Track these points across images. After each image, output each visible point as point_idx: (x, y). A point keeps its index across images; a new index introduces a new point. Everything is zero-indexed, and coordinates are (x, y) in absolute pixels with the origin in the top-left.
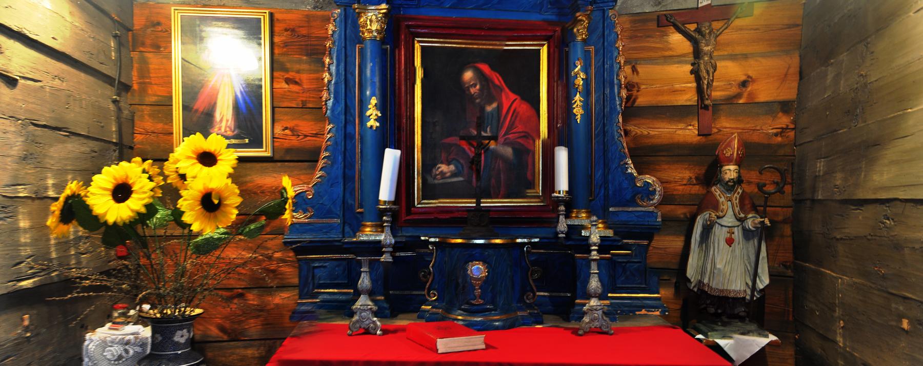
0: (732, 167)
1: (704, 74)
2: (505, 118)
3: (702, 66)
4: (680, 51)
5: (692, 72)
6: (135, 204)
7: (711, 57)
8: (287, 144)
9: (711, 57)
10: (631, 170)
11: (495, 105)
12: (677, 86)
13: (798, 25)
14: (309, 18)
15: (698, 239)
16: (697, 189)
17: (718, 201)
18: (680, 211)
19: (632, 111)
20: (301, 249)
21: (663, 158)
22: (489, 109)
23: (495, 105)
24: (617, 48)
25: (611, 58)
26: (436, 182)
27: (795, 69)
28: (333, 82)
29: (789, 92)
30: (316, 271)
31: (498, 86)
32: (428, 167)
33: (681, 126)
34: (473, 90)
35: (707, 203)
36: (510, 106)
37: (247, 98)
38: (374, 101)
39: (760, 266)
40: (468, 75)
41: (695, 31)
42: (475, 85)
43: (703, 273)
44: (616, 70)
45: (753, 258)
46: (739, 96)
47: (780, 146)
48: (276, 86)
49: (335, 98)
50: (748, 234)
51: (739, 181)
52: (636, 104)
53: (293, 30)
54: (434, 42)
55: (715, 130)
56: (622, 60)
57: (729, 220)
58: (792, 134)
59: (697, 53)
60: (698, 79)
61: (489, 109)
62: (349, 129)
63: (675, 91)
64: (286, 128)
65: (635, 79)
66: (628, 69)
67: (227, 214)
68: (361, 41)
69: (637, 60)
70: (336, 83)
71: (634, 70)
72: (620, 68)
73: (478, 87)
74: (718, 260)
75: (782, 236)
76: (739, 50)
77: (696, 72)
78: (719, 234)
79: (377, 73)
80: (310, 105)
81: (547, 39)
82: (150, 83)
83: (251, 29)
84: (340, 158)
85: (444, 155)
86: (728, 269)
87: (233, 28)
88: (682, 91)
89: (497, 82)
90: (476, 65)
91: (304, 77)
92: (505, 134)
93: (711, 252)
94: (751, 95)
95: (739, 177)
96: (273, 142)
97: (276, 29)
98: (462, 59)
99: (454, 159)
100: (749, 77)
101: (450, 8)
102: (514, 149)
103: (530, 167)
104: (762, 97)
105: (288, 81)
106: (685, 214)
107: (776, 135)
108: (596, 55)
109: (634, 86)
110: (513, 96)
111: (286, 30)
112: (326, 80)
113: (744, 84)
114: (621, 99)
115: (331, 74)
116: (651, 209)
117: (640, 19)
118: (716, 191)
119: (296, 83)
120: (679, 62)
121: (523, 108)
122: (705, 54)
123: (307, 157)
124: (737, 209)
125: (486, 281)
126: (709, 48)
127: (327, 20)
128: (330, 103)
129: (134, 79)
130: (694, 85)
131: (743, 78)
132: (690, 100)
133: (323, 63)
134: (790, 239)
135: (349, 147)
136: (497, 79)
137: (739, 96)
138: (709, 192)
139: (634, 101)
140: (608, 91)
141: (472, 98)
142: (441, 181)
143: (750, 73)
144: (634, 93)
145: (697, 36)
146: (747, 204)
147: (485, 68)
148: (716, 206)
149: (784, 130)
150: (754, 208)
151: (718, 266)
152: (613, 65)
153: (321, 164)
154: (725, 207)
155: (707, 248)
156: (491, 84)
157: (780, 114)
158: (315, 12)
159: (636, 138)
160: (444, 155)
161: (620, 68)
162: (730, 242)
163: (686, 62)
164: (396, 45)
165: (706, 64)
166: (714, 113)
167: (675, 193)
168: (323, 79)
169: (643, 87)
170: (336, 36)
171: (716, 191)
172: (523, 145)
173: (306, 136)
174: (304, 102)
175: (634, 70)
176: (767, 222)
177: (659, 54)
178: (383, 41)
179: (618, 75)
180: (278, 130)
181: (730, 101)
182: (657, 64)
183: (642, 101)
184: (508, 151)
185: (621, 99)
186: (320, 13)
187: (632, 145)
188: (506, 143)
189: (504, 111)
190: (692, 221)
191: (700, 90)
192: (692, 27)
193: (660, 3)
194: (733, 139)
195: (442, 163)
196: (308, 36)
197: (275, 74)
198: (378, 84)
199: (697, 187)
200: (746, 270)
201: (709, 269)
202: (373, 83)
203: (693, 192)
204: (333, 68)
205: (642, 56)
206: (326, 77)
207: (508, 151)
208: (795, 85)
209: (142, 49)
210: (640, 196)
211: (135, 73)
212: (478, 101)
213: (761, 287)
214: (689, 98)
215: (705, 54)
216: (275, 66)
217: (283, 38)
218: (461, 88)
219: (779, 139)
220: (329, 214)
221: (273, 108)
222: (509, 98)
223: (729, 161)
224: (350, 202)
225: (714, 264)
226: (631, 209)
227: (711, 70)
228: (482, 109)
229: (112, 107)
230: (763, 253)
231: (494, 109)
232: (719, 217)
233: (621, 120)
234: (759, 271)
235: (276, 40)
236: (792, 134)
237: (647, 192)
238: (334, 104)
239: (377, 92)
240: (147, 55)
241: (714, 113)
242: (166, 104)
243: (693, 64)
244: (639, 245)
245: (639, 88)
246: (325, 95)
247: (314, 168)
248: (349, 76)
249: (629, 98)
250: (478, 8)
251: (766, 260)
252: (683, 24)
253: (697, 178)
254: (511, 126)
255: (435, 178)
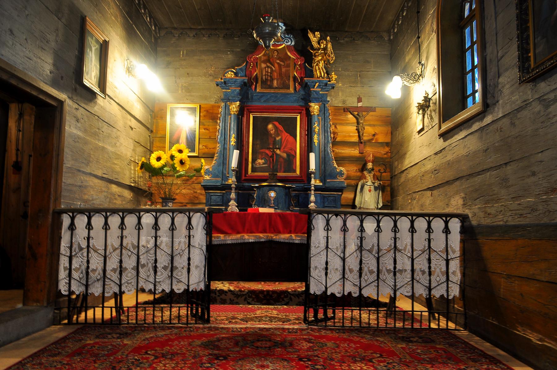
0: (370, 164)
1: (360, 130)
2: (284, 142)
3: (360, 128)
4: (352, 122)
5: (356, 130)
6: (162, 162)
7: (363, 125)
8: (203, 151)
9: (363, 125)
10: (335, 165)
11: (280, 137)
12: (351, 134)
13: (390, 117)
14: (213, 107)
15: (359, 190)
16: (359, 174)
17: (366, 177)
18: (353, 182)
19: (335, 143)
20: (206, 188)
21: (346, 162)
22: (277, 139)
23: (280, 137)
24: (330, 118)
25: (327, 122)
26: (257, 166)
27: (390, 132)
28: (220, 129)
29: (388, 140)
30: (212, 197)
31: (281, 130)
32: (254, 161)
33: (353, 149)
34: (272, 132)
35: (363, 177)
36: (286, 138)
37: (191, 135)
38: (233, 136)
39: (379, 200)
40: (270, 126)
41: (357, 115)
42: (273, 130)
43: (361, 203)
44: (329, 126)
45: (377, 197)
46: (372, 139)
47: (386, 158)
48: (200, 131)
49: (221, 135)
50: (376, 189)
51: (373, 169)
52: (336, 140)
53: (207, 111)
54: (258, 115)
55: (365, 152)
56: (331, 123)
57: (369, 183)
58: (389, 154)
59: (358, 123)
60: (359, 132)
61: (277, 139)
62: (225, 146)
63: (350, 136)
64: (204, 146)
65: (336, 131)
66: (333, 127)
67: (186, 166)
68: (230, 114)
69: (336, 124)
70: (221, 130)
71: (335, 127)
72: (331, 126)
73: (274, 131)
74: (366, 197)
75: (387, 191)
76: (372, 123)
77: (358, 130)
78: (366, 188)
79: (235, 126)
80: (212, 138)
81: (300, 113)
82: (159, 130)
83: (193, 110)
84: (222, 156)
85: (260, 156)
86: (369, 201)
87: (187, 111)
88: (353, 136)
89: (281, 129)
90: (273, 122)
91: (210, 127)
92: (284, 148)
93: (364, 195)
94: (376, 139)
95: (373, 168)
96: (199, 150)
97: (201, 110)
98: (268, 120)
99: (264, 158)
100: (376, 133)
101: (263, 102)
102: (286, 154)
103: (294, 163)
104: (380, 141)
105: (205, 129)
106: (354, 183)
107: (385, 154)
108: (321, 120)
109: (335, 133)
110: (287, 134)
111: (205, 111)
112: (218, 129)
113: (374, 135)
114: (331, 137)
115: (220, 126)
116: (343, 180)
117: (337, 109)
118: (365, 173)
119: (208, 130)
120: (352, 126)
121: (291, 139)
122: (361, 123)
123: (209, 156)
124: (372, 179)
125: (276, 199)
126: (362, 121)
127: (219, 107)
128: (219, 137)
129: (154, 128)
130: (357, 134)
131: (374, 133)
132: (356, 140)
133: (217, 122)
134: (389, 192)
135: (225, 152)
136: (280, 127)
137: (372, 139)
138: (363, 174)
139: (336, 139)
140: (326, 134)
141: (271, 134)
142: (259, 166)
143: (376, 132)
144: (336, 136)
145: (357, 116)
146: (375, 178)
147: (277, 124)
148: (365, 178)
149: (387, 152)
150: (378, 179)
151: (366, 200)
152: (328, 125)
153: (215, 158)
154: (368, 178)
155: (362, 194)
156: (278, 130)
157: (386, 147)
158: (346, 332)
159: (336, 153)
160: (260, 156)
161: (331, 126)
162: (370, 191)
163: (354, 126)
164: (243, 116)
165: (361, 127)
166: (365, 145)
167: (351, 175)
168: (217, 128)
169: (339, 134)
170: (222, 113)
171: (365, 173)
172: (290, 153)
173: (210, 148)
174: (210, 137)
175: (335, 127)
176: (381, 182)
177: (345, 122)
178: (238, 115)
179: (330, 129)
180: (201, 147)
181: (370, 141)
182: (344, 125)
183: (338, 139)
184: (285, 155)
185: (331, 137)
186: (217, 104)
187: (335, 156)
188: (284, 152)
189: (283, 140)
190: (357, 186)
191: (359, 136)
192: (356, 113)
193: (344, 103)
194: (371, 154)
195: (259, 159)
196: (212, 113)
197: (200, 126)
198: (235, 130)
199: (359, 173)
200: (375, 202)
201: (363, 202)
202: (234, 129)
203: (357, 175)
204: (221, 124)
205: (338, 122)
206: (218, 127)
207: (285, 155)
208: (390, 137)
209: (157, 118)
210: (338, 175)
211: (154, 127)
212: (273, 136)
213: (380, 207)
214: (356, 139)
215: (361, 123)
216: (201, 124)
217: (204, 114)
218: (267, 132)
219: (386, 156)
220: (217, 176)
221: (199, 139)
222: (285, 135)
223: (369, 161)
224: (225, 172)
225: (365, 199)
226: (335, 180)
227: (363, 129)
228: (275, 139)
229: (149, 137)
230: (380, 195)
231: (279, 139)
232: (366, 182)
233: (331, 146)
234: (379, 201)
235: (201, 114)
236: (389, 154)
237: (341, 174)
238: (220, 137)
239: (235, 133)
240: (159, 120)
241: (365, 145)
242: (164, 137)
243: (357, 127)
244: (338, 194)
245: (337, 134)
246: (217, 134)
247: (212, 160)
248: (226, 127)
249: (334, 138)
250: (274, 102)
251: (381, 198)
252: (353, 112)
253: (359, 170)
254: (285, 146)
255: (256, 165)
